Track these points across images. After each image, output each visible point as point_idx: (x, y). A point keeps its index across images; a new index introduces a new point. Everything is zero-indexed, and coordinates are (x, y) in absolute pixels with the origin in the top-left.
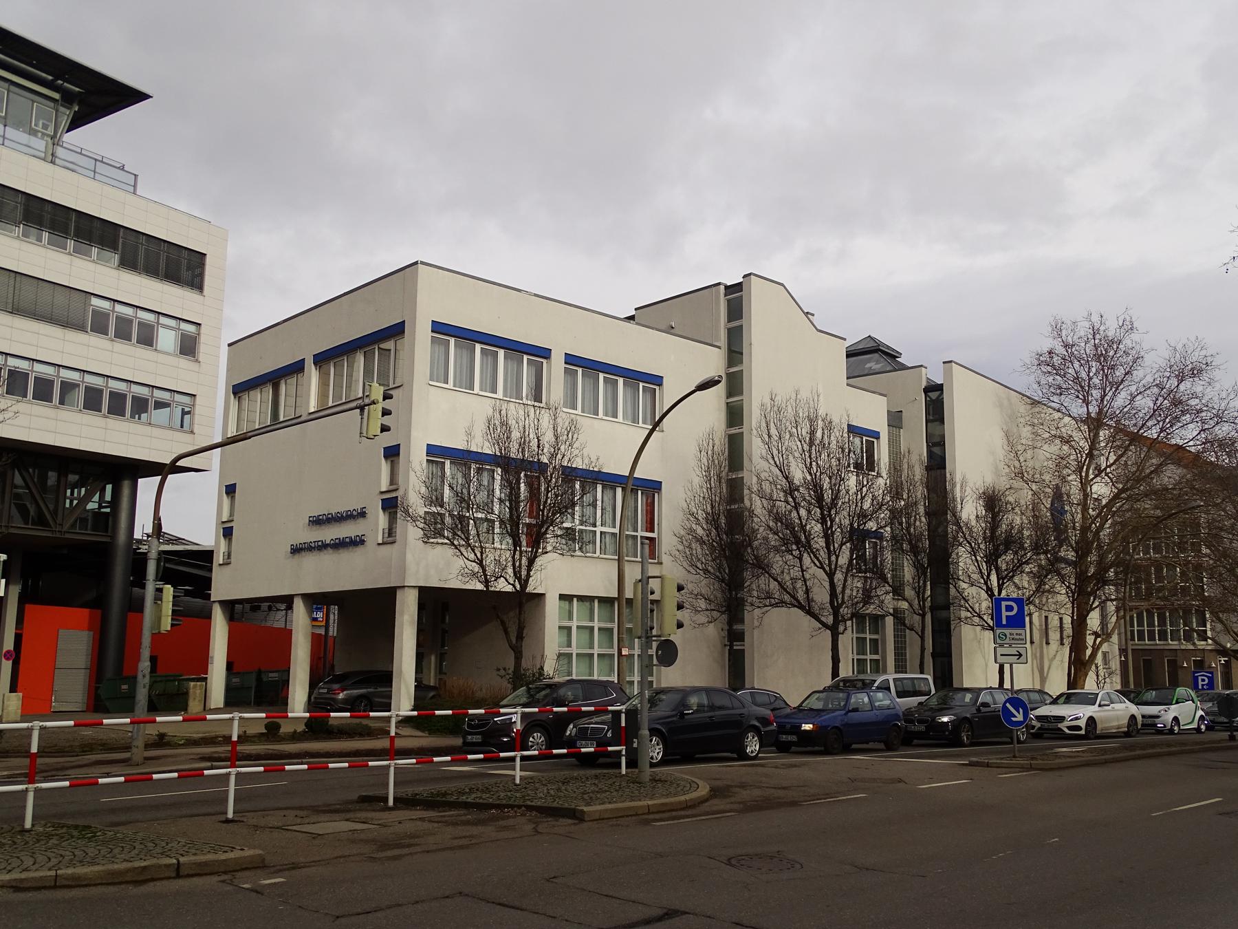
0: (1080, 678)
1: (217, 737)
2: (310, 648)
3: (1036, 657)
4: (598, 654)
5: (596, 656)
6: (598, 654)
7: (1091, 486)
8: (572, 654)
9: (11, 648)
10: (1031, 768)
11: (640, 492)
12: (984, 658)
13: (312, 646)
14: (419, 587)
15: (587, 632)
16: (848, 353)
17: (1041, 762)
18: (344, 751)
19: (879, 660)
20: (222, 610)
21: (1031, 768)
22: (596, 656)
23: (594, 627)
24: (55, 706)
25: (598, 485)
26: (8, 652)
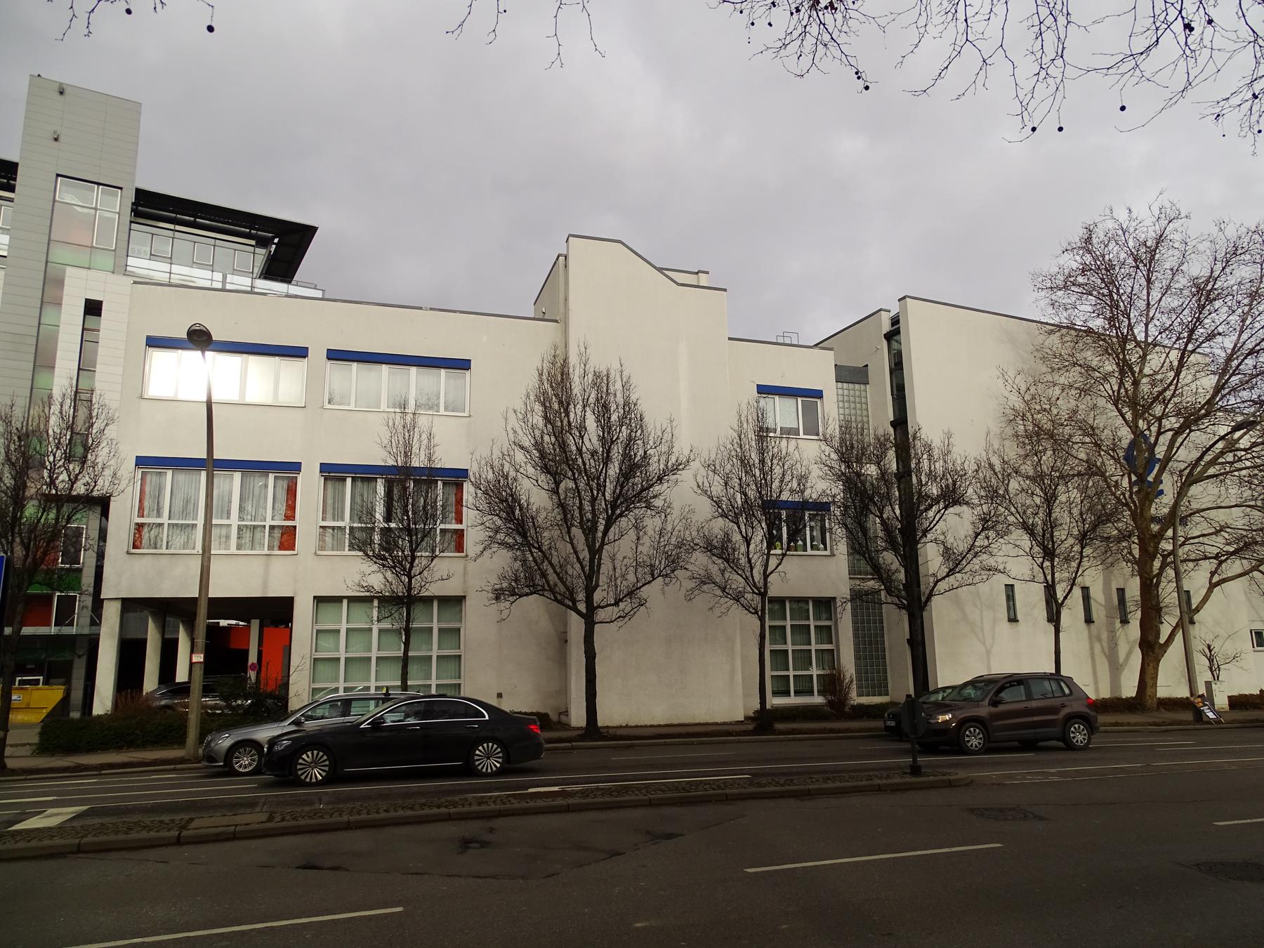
0: (1149, 665)
1: (733, 732)
2: (159, 660)
3: (1099, 640)
4: (816, 650)
5: (434, 659)
6: (438, 656)
7: (1191, 431)
8: (787, 650)
9: (255, 661)
10: (880, 789)
11: (349, 481)
12: (984, 643)
13: (161, 659)
14: (122, 598)
15: (319, 635)
16: (893, 321)
17: (932, 778)
18: (34, 767)
19: (833, 650)
20: (154, 622)
21: (880, 789)
22: (434, 659)
23: (432, 627)
24: (352, 713)
25: (378, 479)
26: (253, 664)
